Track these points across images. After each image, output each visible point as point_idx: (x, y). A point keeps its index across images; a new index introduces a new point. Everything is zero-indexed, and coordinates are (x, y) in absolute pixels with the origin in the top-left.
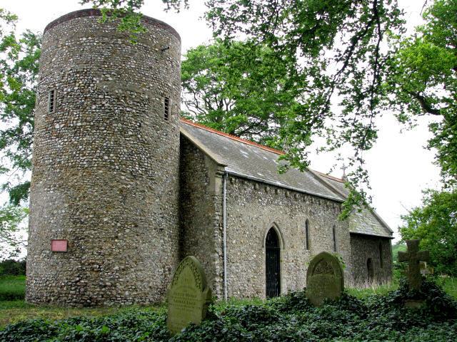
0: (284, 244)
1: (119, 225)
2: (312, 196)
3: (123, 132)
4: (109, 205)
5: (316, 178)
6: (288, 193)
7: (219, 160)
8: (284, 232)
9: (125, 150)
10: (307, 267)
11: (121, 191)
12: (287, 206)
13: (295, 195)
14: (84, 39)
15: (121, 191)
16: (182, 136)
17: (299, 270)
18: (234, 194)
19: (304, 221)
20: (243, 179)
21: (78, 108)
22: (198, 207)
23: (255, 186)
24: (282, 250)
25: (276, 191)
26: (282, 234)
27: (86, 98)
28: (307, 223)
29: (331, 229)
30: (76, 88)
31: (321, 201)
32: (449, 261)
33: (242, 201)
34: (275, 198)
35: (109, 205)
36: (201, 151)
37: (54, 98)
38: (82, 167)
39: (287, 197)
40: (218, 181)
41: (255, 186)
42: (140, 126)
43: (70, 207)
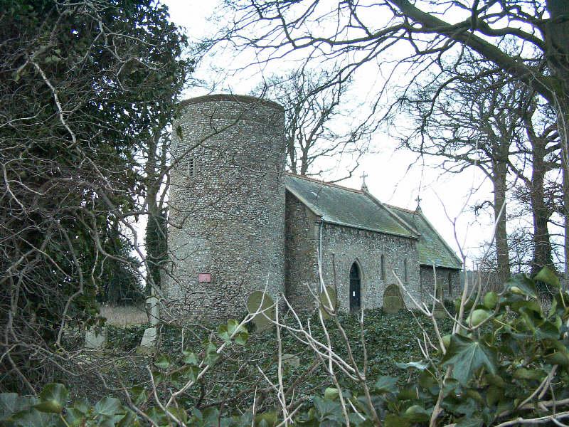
0: (364, 275)
1: (248, 262)
2: (387, 234)
3: (249, 194)
4: (241, 249)
5: (302, 38)
6: (367, 233)
7: (317, 212)
8: (363, 266)
9: (251, 207)
10: (382, 292)
11: (249, 237)
12: (366, 244)
13: (373, 235)
14: (217, 120)
15: (249, 237)
16: (287, 190)
17: (375, 297)
18: (327, 238)
19: (380, 256)
20: (334, 225)
21: (214, 175)
22: (300, 248)
23: (342, 229)
24: (362, 280)
25: (358, 232)
26: (362, 267)
27: (221, 167)
28: (382, 257)
29: (403, 262)
30: (212, 159)
31: (395, 238)
32: (534, 2)
33: (333, 243)
34: (358, 238)
35: (241, 249)
36: (303, 204)
37: (194, 164)
38: (220, 219)
39: (367, 237)
40: (316, 228)
41: (342, 229)
42: (260, 188)
43: (212, 249)
